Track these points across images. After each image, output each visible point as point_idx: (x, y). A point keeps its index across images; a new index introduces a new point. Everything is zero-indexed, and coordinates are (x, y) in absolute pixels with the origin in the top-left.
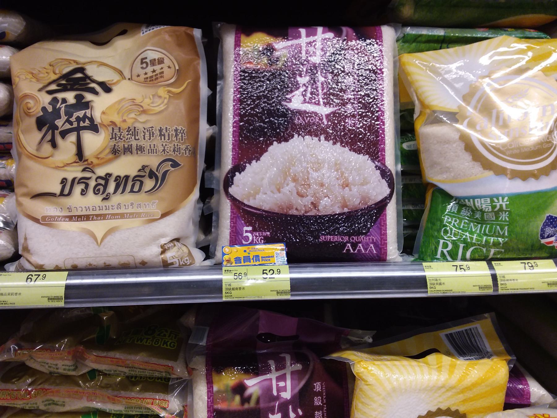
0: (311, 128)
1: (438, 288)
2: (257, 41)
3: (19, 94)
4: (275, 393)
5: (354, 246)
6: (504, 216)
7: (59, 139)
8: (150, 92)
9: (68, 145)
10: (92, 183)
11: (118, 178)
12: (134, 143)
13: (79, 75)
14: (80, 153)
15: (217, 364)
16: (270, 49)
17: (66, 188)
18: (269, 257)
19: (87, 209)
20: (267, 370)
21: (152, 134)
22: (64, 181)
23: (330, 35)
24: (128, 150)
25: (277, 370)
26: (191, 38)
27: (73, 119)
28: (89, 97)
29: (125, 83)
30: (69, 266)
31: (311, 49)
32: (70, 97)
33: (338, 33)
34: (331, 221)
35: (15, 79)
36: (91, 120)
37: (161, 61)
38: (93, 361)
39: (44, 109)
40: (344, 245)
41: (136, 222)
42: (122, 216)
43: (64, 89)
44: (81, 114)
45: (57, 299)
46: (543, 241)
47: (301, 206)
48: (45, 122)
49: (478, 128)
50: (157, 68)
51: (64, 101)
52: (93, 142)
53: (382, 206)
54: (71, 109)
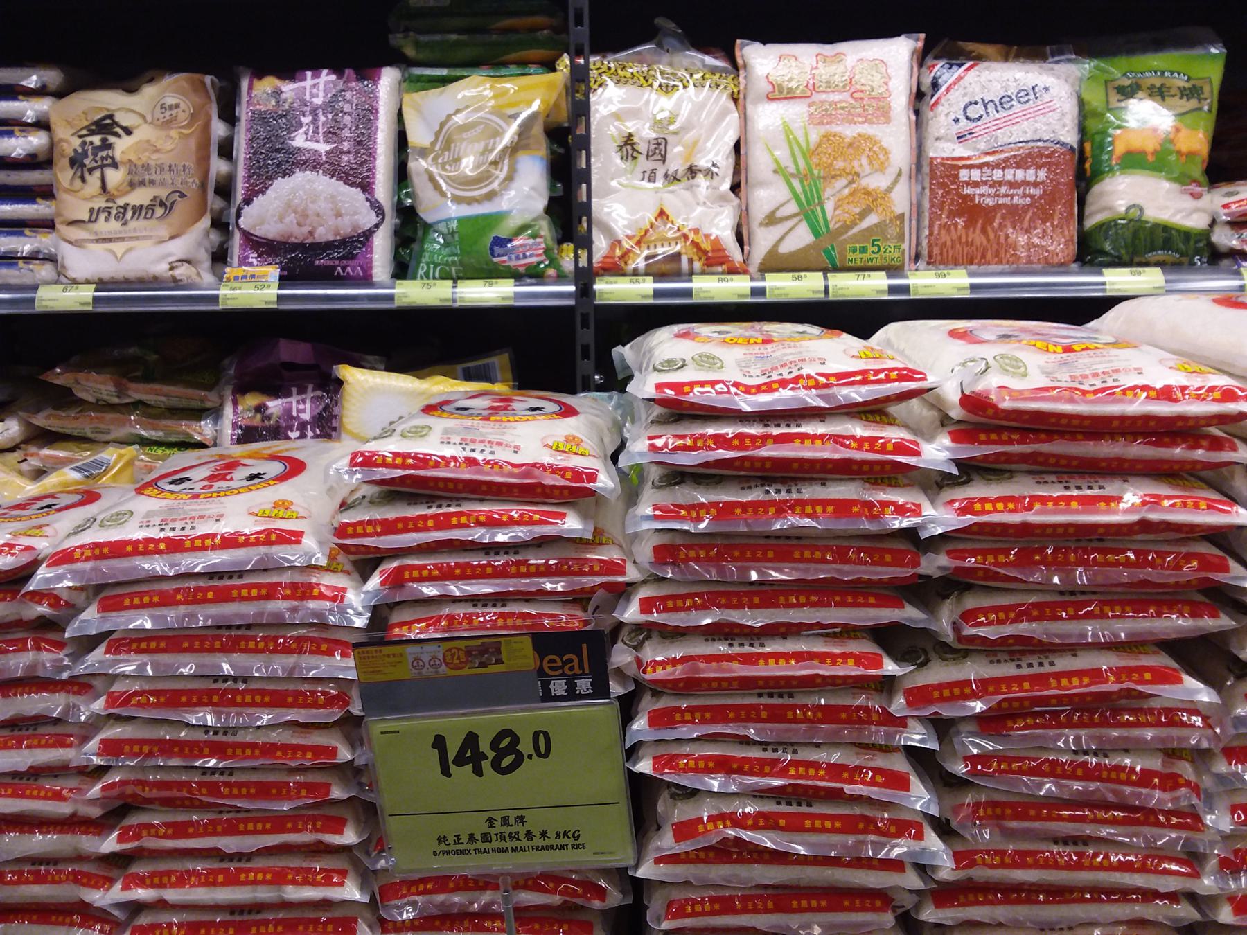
0: (312, 163)
1: (404, 300)
2: (268, 84)
3: (56, 139)
4: (294, 414)
5: (344, 269)
6: (457, 237)
7: (87, 175)
8: (162, 133)
9: (94, 180)
10: (114, 212)
11: (134, 208)
12: (147, 177)
13: (108, 121)
14: (104, 187)
15: (242, 389)
16: (277, 93)
17: (94, 215)
19: (110, 232)
20: (289, 395)
21: (162, 170)
22: (91, 210)
23: (333, 77)
24: (142, 183)
25: (298, 394)
26: (203, 84)
27: (98, 158)
28: (112, 139)
29: (146, 126)
30: (96, 279)
31: (315, 91)
32: (97, 140)
33: (340, 74)
34: (328, 246)
35: (53, 126)
36: (113, 158)
37: (177, 106)
38: (138, 392)
39: (75, 150)
40: (334, 268)
41: (149, 243)
42: (137, 238)
43: (92, 133)
44: (104, 154)
45: (87, 304)
46: (495, 260)
47: (299, 234)
48: (76, 162)
50: (174, 112)
51: (91, 143)
52: (115, 177)
53: (368, 234)
54: (97, 150)
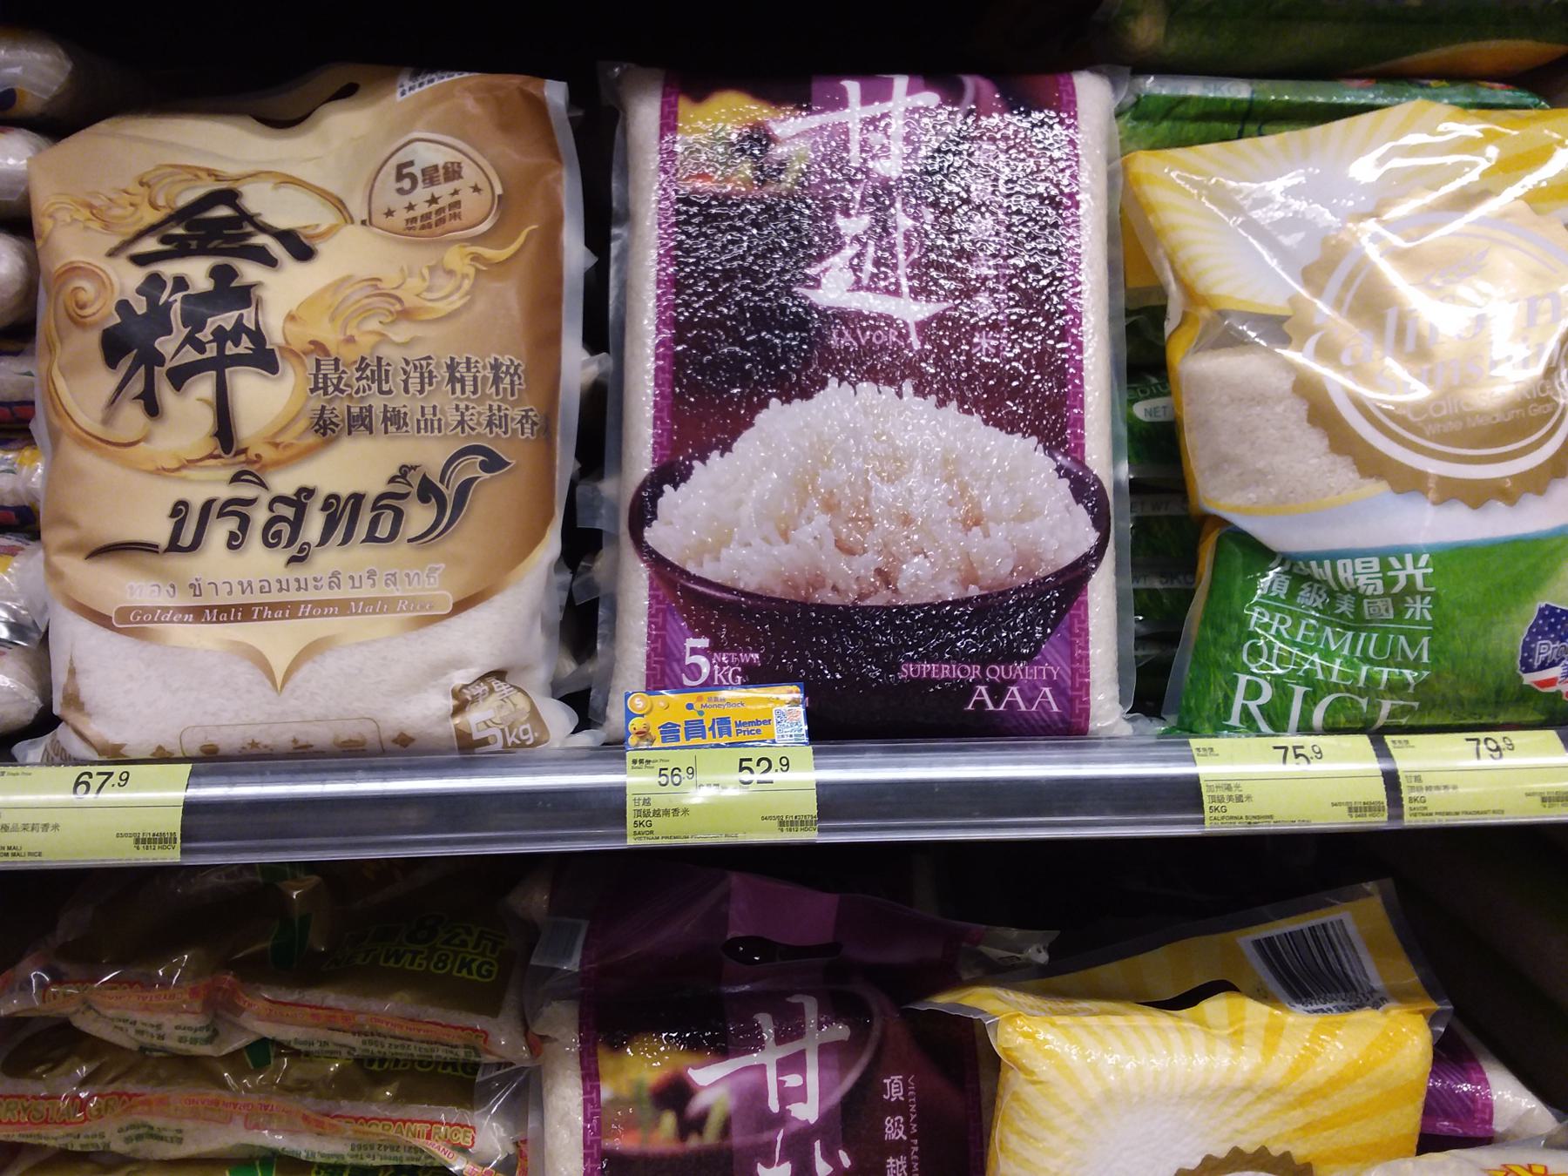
0: (874, 359)
1: (1234, 809)
2: (724, 117)
3: (53, 264)
4: (774, 1105)
5: (997, 691)
6: (1419, 609)
7: (165, 392)
8: (421, 257)
9: (191, 408)
10: (260, 516)
11: (331, 502)
12: (377, 403)
13: (223, 211)
14: (225, 431)
15: (610, 1025)
16: (760, 138)
17: (187, 530)
18: (757, 723)
19: (246, 587)
20: (753, 1042)
21: (427, 378)
22: (179, 510)
23: (930, 98)
24: (360, 422)
25: (780, 1040)
26: (539, 106)
27: (205, 335)
28: (249, 272)
29: (353, 233)
30: (194, 749)
31: (876, 138)
32: (197, 272)
33: (953, 94)
34: (932, 623)
35: (43, 223)
36: (257, 336)
37: (452, 172)
38: (262, 1016)
39: (124, 306)
40: (970, 689)
41: (382, 625)
42: (344, 608)
43: (181, 250)
44: (227, 320)
45: (162, 840)
46: (1529, 679)
47: (847, 578)
48: (126, 344)
49: (1346, 359)
50: (443, 190)
51: (181, 283)
52: (262, 401)
53: (1074, 578)
54: (199, 307)
